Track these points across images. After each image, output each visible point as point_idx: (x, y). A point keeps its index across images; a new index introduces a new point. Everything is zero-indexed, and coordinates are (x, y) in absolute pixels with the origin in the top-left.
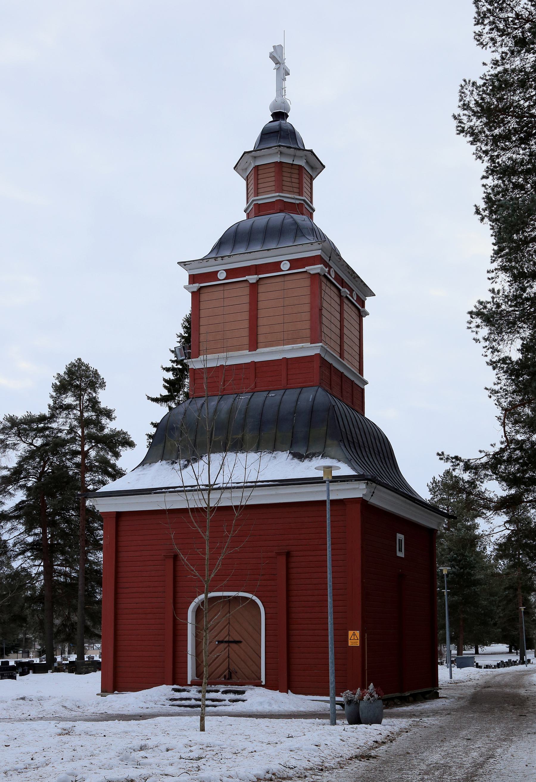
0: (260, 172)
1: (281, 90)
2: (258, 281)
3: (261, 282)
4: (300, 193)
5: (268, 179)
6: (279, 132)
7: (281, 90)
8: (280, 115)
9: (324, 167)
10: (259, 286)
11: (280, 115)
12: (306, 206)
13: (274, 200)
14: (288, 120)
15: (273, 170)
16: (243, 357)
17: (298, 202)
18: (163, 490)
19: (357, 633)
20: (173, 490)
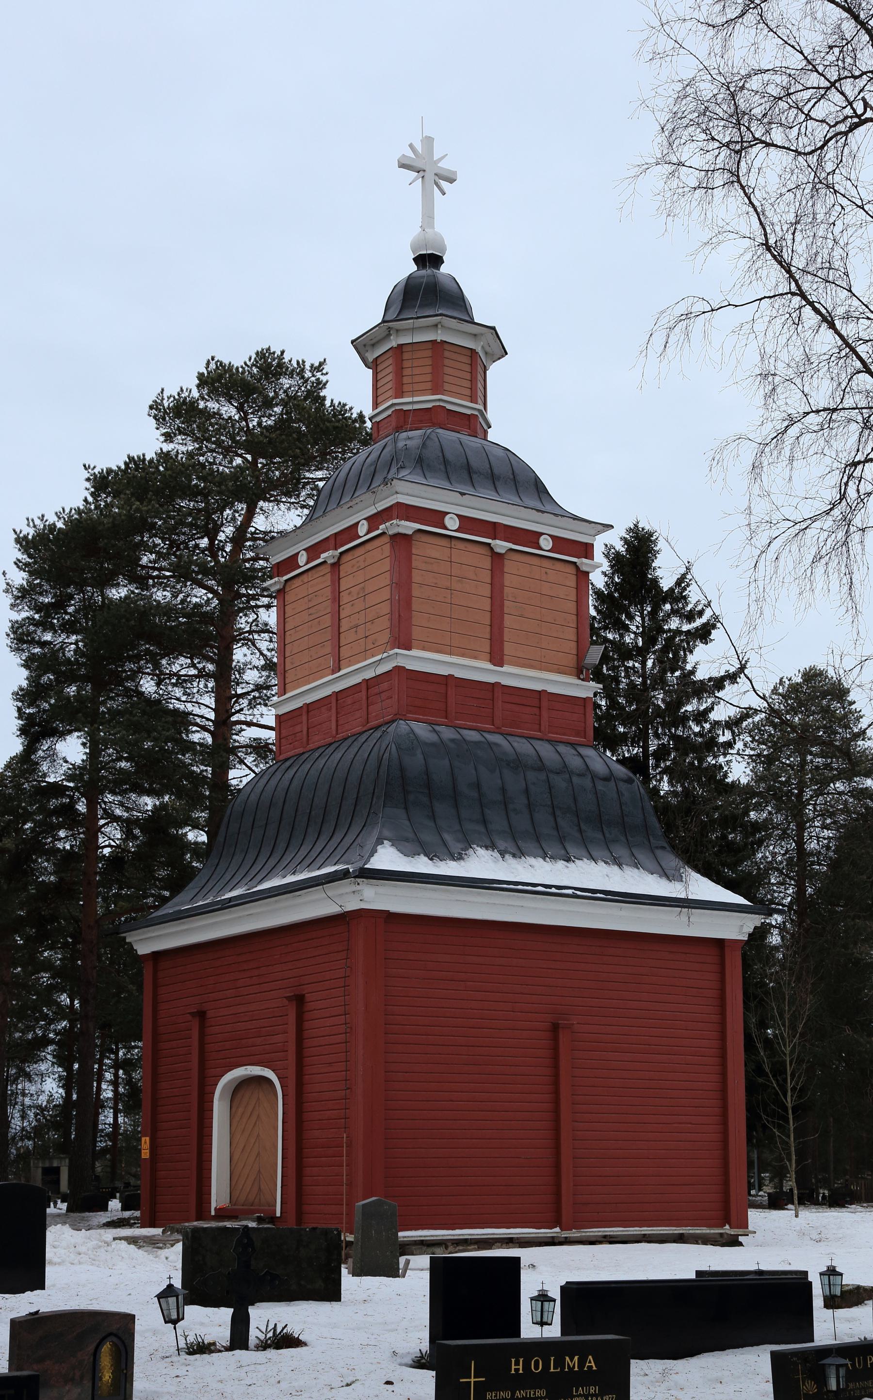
0: (406, 356)
1: (428, 216)
2: (339, 559)
3: (345, 558)
4: (473, 399)
5: (419, 368)
6: (427, 291)
7: (428, 216)
8: (429, 260)
9: (506, 354)
10: (341, 567)
11: (429, 260)
12: (481, 420)
13: (429, 405)
14: (444, 269)
15: (390, 361)
16: (478, 670)
17: (469, 412)
18: (520, 887)
19: (148, 1139)
20: (579, 893)
